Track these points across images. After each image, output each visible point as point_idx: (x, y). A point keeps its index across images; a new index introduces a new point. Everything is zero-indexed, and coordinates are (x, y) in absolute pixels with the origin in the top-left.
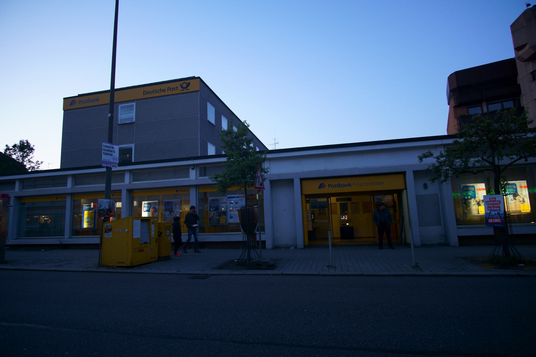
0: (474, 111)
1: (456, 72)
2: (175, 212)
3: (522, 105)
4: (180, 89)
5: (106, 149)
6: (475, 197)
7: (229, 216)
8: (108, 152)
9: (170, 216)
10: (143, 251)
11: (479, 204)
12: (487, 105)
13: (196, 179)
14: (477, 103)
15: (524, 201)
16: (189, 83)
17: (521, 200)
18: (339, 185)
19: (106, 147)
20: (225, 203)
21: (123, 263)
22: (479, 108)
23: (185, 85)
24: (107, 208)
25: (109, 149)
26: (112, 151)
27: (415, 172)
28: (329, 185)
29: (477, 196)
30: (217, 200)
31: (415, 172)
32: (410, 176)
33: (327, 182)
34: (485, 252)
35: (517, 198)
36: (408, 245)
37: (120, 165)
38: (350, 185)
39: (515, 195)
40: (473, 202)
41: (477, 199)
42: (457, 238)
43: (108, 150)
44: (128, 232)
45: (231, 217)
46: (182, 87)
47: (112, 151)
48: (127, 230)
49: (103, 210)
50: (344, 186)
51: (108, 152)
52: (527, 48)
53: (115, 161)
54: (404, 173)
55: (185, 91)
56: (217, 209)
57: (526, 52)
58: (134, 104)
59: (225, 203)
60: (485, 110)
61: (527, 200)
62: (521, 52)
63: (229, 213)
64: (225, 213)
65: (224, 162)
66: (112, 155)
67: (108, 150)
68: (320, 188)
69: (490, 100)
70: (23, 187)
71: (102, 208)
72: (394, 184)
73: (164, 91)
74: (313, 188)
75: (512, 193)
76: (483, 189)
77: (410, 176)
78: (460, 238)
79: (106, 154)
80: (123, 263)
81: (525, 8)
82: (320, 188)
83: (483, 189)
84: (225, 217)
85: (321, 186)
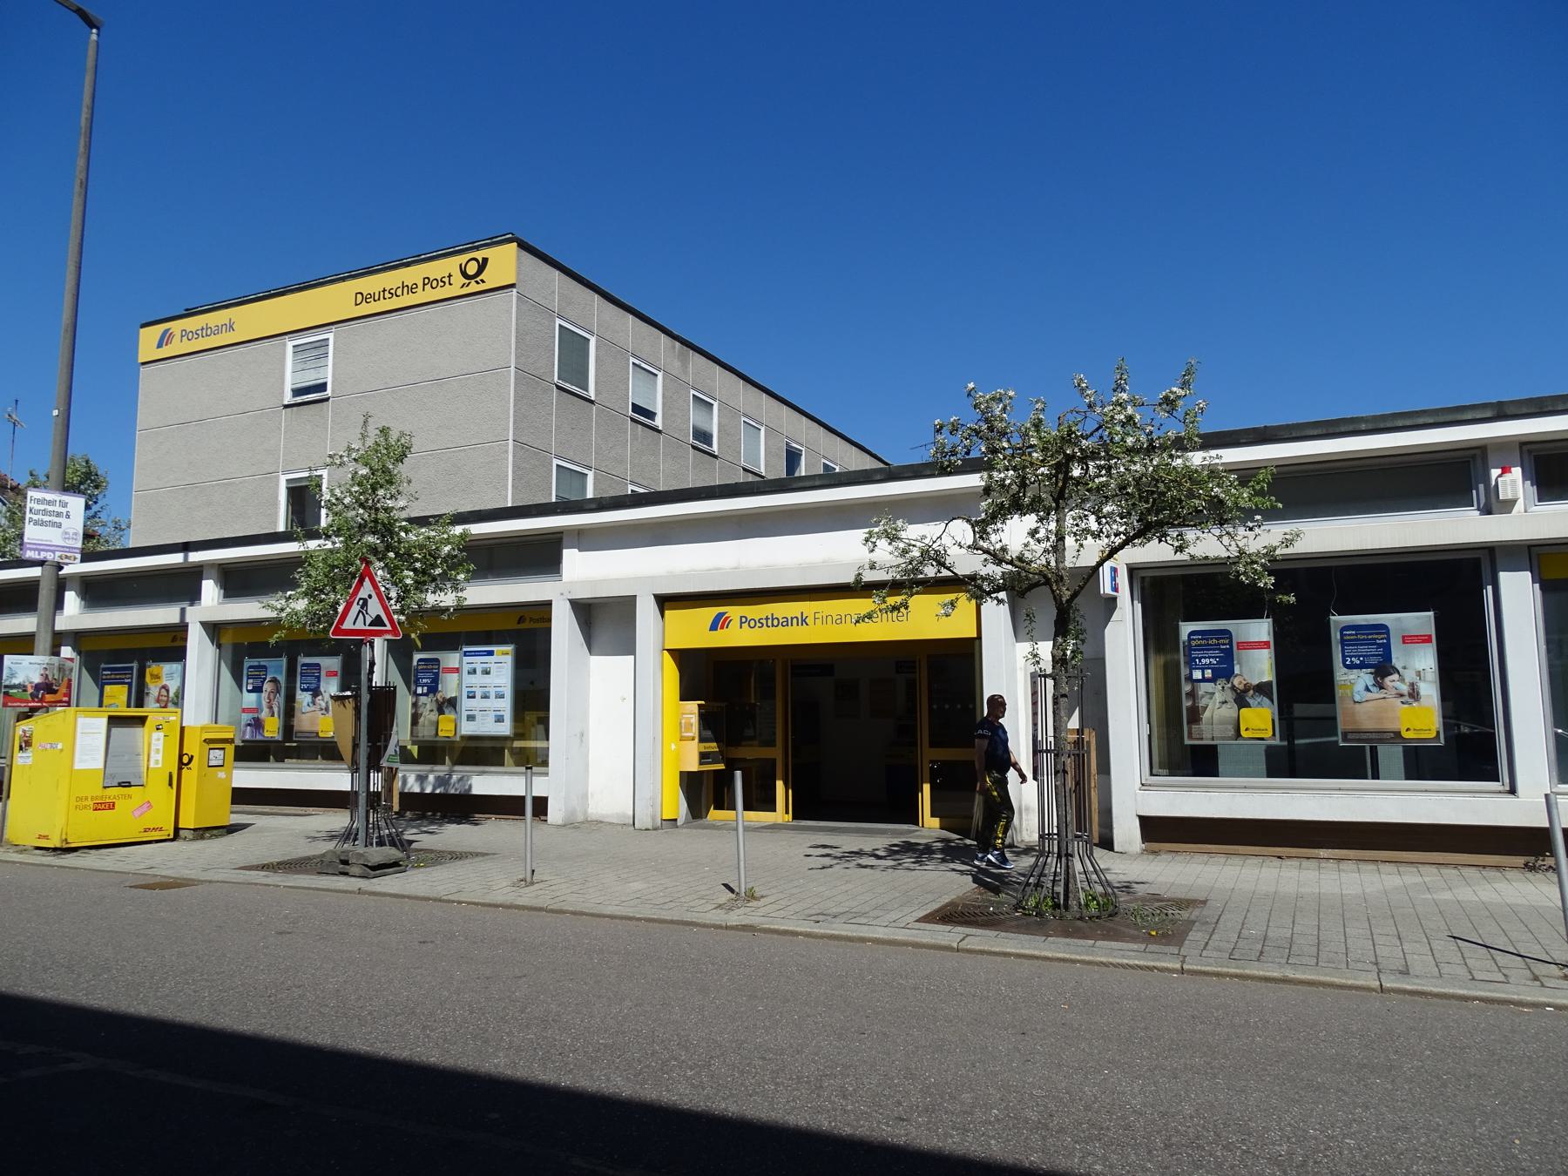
2: (1409, 676)
4: (458, 279)
5: (42, 507)
7: (464, 714)
8: (46, 518)
9: (1376, 693)
10: (112, 806)
11: (1241, 701)
15: (1414, 694)
16: (485, 260)
17: (1405, 688)
18: (772, 622)
19: (38, 501)
20: (457, 670)
21: (46, 837)
23: (472, 269)
24: (37, 680)
25: (50, 508)
26: (59, 515)
28: (743, 620)
29: (1237, 670)
33: (734, 612)
35: (1388, 680)
37: (87, 557)
38: (804, 621)
41: (439, 696)
43: (45, 512)
45: (471, 718)
46: (464, 274)
47: (59, 515)
49: (23, 688)
50: (787, 622)
51: (46, 518)
53: (70, 543)
55: (474, 287)
58: (331, 336)
59: (457, 670)
61: (1430, 691)
63: (466, 704)
64: (452, 703)
66: (59, 526)
67: (45, 512)
68: (713, 627)
71: (15, 681)
73: (412, 289)
74: (693, 629)
75: (1374, 661)
76: (1266, 645)
79: (36, 523)
80: (46, 837)
82: (713, 627)
83: (1266, 645)
84: (453, 716)
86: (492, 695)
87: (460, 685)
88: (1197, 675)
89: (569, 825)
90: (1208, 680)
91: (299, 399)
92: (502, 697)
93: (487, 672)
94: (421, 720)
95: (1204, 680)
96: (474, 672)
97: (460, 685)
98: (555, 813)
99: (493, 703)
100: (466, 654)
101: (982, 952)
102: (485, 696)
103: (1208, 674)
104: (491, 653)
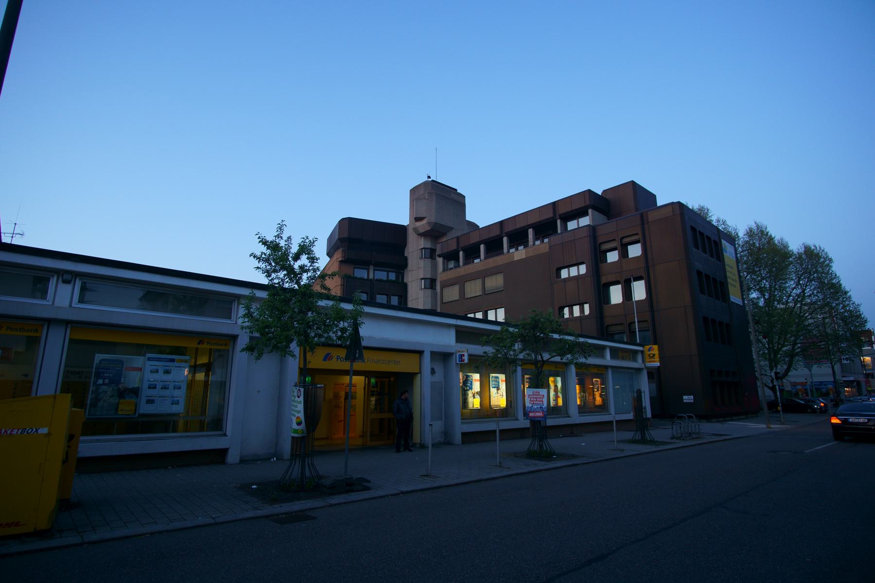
0: (361, 273)
1: (350, 219)
3: (405, 281)
6: (471, 388)
7: (143, 400)
12: (374, 270)
13: (70, 306)
14: (364, 264)
20: (140, 369)
21: (17, 524)
22: (366, 271)
27: (432, 353)
30: (121, 362)
31: (432, 353)
32: (427, 357)
34: (523, 445)
36: (423, 446)
39: (498, 389)
40: (470, 394)
42: (460, 435)
44: (49, 434)
45: (150, 401)
48: (44, 431)
52: (425, 222)
54: (420, 353)
56: (115, 381)
57: (423, 225)
60: (371, 277)
62: (418, 224)
63: (146, 393)
64: (135, 392)
65: (496, 332)
68: (325, 359)
69: (379, 266)
70: (613, 357)
72: (404, 365)
77: (427, 357)
78: (464, 434)
80: (17, 524)
81: (426, 179)
82: (325, 359)
85: (328, 357)
86: (171, 387)
87: (142, 380)
88: (100, 381)
89: (243, 461)
90: (106, 385)
91: (689, 230)
92: (180, 388)
93: (167, 372)
94: (100, 404)
95: (104, 384)
96: (157, 371)
97: (142, 380)
98: (233, 457)
99: (177, 393)
100: (149, 359)
101: (613, 459)
102: (165, 388)
103: (107, 381)
104: (173, 360)
